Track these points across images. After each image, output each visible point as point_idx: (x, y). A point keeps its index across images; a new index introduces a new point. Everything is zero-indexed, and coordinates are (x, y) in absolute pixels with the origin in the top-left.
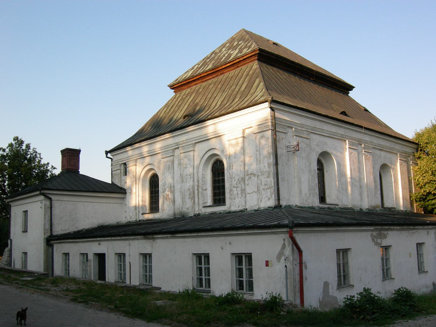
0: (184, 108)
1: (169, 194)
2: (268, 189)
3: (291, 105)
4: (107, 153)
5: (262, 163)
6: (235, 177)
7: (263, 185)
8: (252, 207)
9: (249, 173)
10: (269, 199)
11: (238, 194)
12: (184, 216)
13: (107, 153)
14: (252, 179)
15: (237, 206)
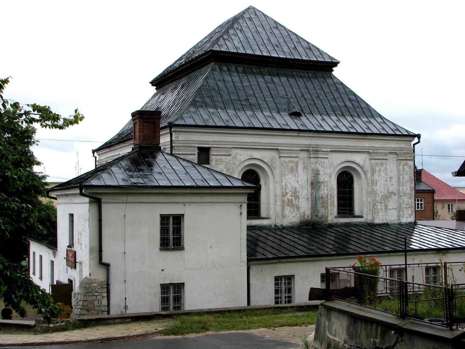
1: (292, 199)
2: (409, 208)
4: (94, 152)
5: (404, 186)
6: (379, 194)
7: (405, 204)
8: (392, 221)
11: (382, 209)
13: (94, 152)
14: (392, 197)
15: (381, 219)
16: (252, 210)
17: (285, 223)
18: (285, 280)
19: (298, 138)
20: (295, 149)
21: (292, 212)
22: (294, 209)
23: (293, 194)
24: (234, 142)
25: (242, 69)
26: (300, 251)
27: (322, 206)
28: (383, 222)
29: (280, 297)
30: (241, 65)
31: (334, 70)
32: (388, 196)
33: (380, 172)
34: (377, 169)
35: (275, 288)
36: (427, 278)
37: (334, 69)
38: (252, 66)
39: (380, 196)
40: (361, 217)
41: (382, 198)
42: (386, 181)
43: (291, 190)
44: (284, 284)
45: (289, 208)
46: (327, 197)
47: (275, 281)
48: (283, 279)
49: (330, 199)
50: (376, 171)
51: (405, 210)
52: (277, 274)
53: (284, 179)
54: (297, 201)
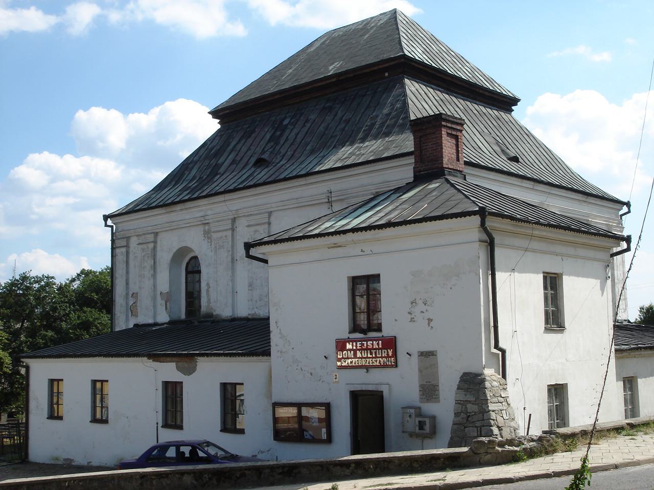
0: (259, 222)
3: (431, 66)
4: (106, 218)
13: (106, 218)
31: (513, 110)
37: (513, 108)
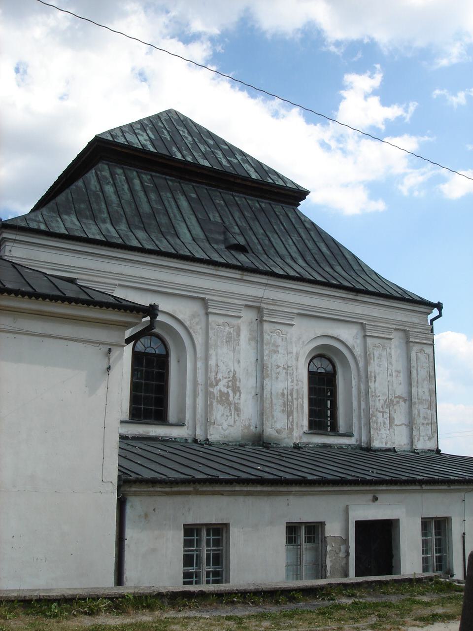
1: (228, 392)
2: (428, 424)
5: (420, 386)
6: (379, 396)
7: (421, 418)
8: (401, 445)
9: (397, 395)
10: (429, 439)
11: (384, 423)
12: (270, 444)
14: (400, 404)
15: (384, 441)
16: (152, 409)
17: (213, 436)
18: (208, 535)
19: (242, 284)
20: (237, 302)
21: (227, 416)
22: (230, 410)
23: (230, 384)
24: (122, 274)
25: (149, 177)
26: (240, 459)
27: (283, 410)
28: (386, 447)
29: (196, 573)
30: (148, 172)
32: (395, 403)
33: (381, 359)
34: (376, 353)
35: (185, 551)
36: (425, 560)
38: (167, 177)
39: (381, 401)
40: (349, 435)
41: (385, 404)
42: (391, 375)
43: (226, 375)
44: (207, 545)
45: (221, 408)
46: (291, 394)
47: (185, 535)
48: (204, 533)
49: (297, 399)
50: (374, 358)
51: (422, 428)
52: (191, 519)
53: (214, 353)
54: (237, 397)
